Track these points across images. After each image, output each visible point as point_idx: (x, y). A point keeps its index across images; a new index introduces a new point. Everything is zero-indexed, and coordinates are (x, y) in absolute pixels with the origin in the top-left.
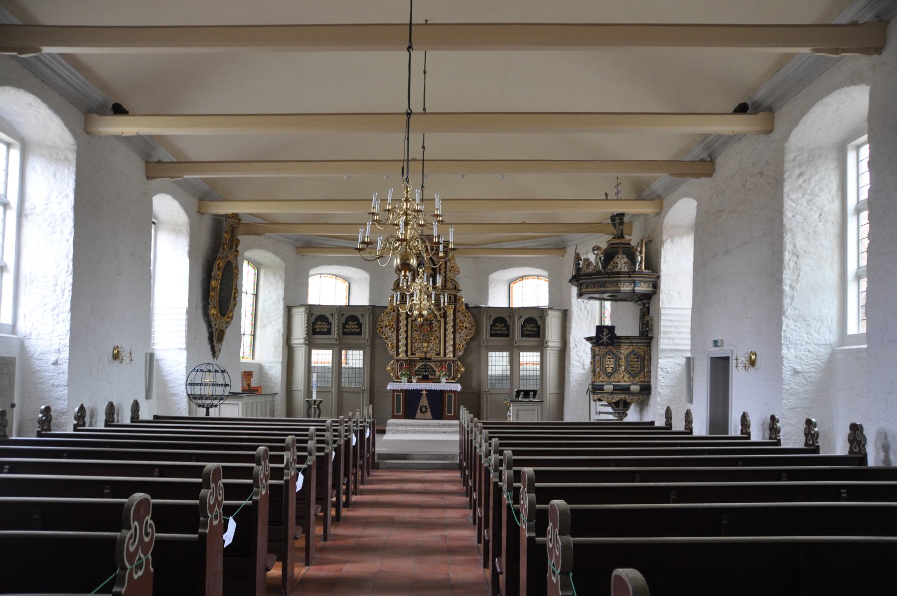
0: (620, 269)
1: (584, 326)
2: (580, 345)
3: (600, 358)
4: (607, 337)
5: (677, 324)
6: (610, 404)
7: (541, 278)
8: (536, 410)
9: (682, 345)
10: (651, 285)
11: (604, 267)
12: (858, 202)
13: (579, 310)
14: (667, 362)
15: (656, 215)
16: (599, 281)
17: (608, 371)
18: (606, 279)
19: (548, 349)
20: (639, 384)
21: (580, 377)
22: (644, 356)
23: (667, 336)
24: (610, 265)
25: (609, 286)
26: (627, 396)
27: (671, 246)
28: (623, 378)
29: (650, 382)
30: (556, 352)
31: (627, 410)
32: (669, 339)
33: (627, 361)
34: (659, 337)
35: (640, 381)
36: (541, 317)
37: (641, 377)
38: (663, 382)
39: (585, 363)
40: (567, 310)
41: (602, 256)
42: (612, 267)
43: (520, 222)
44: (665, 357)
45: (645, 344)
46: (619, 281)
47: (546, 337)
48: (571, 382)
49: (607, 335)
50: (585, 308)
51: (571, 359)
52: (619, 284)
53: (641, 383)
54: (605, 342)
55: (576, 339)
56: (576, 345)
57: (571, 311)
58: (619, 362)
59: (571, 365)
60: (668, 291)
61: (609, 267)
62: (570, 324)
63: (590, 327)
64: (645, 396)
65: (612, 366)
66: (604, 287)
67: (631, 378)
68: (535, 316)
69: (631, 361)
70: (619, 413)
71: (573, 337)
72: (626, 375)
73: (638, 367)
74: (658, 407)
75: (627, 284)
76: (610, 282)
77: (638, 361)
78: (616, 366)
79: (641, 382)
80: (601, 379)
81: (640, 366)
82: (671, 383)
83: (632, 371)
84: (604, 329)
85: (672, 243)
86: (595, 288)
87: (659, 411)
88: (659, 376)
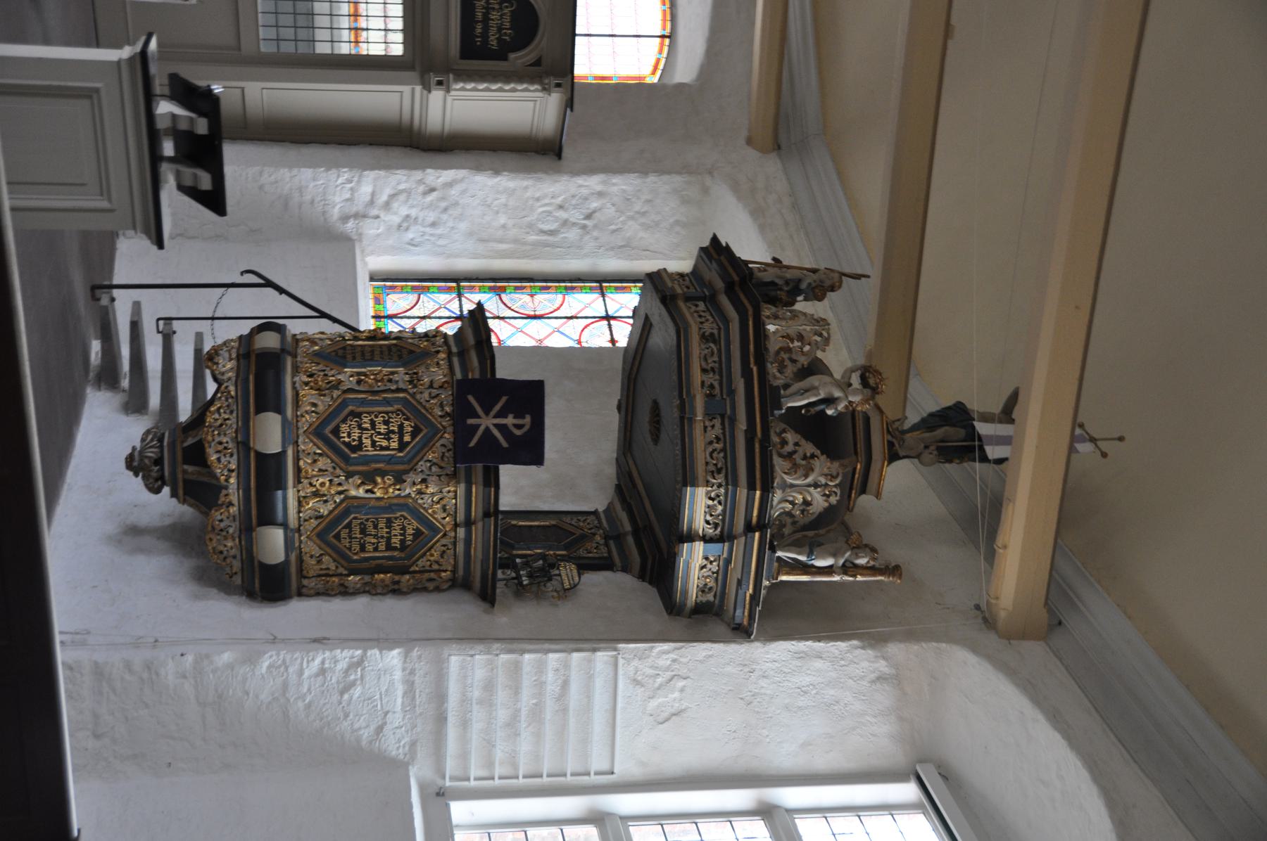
0: (785, 486)
1: (502, 219)
2: (431, 206)
3: (398, 390)
4: (496, 432)
5: (548, 715)
6: (202, 409)
7: (666, 49)
8: (104, 204)
9: (464, 740)
10: (710, 597)
11: (797, 419)
12: (792, 812)
13: (559, 200)
14: (392, 683)
15: (984, 607)
16: (732, 393)
17: (344, 428)
18: (742, 425)
19: (418, 88)
20: (293, 557)
21: (312, 202)
22: (414, 568)
23: (501, 679)
24: (798, 437)
25: (712, 435)
26: (233, 510)
27: (862, 678)
28: (316, 494)
29: (300, 594)
30: (406, 116)
31: (174, 494)
32: (489, 686)
33: (390, 508)
34: (497, 646)
35: (307, 558)
36: (538, 63)
37: (319, 562)
38: (301, 672)
39: (369, 221)
40: (559, 155)
41: (841, 407)
42: (789, 448)
43: (954, 21)
44: (412, 672)
45: (461, 572)
46: (732, 480)
47: (464, 81)
48: (295, 171)
49: (502, 428)
50: (565, 223)
51: (382, 173)
52: (720, 479)
53: (293, 569)
54: (470, 421)
55: (454, 192)
56: (433, 190)
57: (559, 171)
58: (383, 474)
59: (355, 174)
60: (684, 672)
61: (790, 437)
62: (511, 171)
63: (501, 241)
64: (238, 580)
65: (367, 442)
66: (709, 415)
67: (314, 522)
68: (543, 43)
69: (389, 523)
70: (158, 462)
71: (462, 180)
72: (330, 506)
73: (363, 549)
74: (190, 658)
75: (720, 508)
76: (727, 440)
77: (389, 547)
78: (367, 460)
79: (300, 560)
80: (308, 395)
81: (367, 559)
82: (300, 704)
83: (349, 526)
84: (528, 420)
85: (873, 682)
86: (704, 371)
87: (171, 663)
88: (327, 654)
